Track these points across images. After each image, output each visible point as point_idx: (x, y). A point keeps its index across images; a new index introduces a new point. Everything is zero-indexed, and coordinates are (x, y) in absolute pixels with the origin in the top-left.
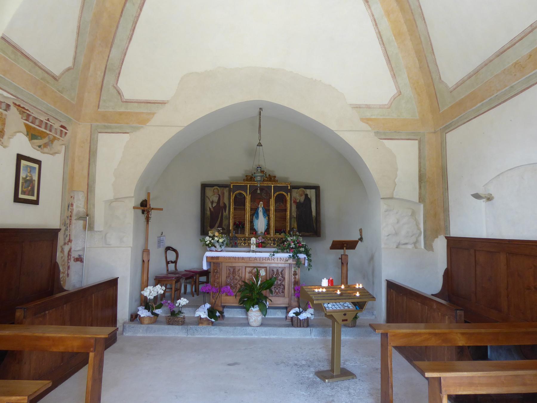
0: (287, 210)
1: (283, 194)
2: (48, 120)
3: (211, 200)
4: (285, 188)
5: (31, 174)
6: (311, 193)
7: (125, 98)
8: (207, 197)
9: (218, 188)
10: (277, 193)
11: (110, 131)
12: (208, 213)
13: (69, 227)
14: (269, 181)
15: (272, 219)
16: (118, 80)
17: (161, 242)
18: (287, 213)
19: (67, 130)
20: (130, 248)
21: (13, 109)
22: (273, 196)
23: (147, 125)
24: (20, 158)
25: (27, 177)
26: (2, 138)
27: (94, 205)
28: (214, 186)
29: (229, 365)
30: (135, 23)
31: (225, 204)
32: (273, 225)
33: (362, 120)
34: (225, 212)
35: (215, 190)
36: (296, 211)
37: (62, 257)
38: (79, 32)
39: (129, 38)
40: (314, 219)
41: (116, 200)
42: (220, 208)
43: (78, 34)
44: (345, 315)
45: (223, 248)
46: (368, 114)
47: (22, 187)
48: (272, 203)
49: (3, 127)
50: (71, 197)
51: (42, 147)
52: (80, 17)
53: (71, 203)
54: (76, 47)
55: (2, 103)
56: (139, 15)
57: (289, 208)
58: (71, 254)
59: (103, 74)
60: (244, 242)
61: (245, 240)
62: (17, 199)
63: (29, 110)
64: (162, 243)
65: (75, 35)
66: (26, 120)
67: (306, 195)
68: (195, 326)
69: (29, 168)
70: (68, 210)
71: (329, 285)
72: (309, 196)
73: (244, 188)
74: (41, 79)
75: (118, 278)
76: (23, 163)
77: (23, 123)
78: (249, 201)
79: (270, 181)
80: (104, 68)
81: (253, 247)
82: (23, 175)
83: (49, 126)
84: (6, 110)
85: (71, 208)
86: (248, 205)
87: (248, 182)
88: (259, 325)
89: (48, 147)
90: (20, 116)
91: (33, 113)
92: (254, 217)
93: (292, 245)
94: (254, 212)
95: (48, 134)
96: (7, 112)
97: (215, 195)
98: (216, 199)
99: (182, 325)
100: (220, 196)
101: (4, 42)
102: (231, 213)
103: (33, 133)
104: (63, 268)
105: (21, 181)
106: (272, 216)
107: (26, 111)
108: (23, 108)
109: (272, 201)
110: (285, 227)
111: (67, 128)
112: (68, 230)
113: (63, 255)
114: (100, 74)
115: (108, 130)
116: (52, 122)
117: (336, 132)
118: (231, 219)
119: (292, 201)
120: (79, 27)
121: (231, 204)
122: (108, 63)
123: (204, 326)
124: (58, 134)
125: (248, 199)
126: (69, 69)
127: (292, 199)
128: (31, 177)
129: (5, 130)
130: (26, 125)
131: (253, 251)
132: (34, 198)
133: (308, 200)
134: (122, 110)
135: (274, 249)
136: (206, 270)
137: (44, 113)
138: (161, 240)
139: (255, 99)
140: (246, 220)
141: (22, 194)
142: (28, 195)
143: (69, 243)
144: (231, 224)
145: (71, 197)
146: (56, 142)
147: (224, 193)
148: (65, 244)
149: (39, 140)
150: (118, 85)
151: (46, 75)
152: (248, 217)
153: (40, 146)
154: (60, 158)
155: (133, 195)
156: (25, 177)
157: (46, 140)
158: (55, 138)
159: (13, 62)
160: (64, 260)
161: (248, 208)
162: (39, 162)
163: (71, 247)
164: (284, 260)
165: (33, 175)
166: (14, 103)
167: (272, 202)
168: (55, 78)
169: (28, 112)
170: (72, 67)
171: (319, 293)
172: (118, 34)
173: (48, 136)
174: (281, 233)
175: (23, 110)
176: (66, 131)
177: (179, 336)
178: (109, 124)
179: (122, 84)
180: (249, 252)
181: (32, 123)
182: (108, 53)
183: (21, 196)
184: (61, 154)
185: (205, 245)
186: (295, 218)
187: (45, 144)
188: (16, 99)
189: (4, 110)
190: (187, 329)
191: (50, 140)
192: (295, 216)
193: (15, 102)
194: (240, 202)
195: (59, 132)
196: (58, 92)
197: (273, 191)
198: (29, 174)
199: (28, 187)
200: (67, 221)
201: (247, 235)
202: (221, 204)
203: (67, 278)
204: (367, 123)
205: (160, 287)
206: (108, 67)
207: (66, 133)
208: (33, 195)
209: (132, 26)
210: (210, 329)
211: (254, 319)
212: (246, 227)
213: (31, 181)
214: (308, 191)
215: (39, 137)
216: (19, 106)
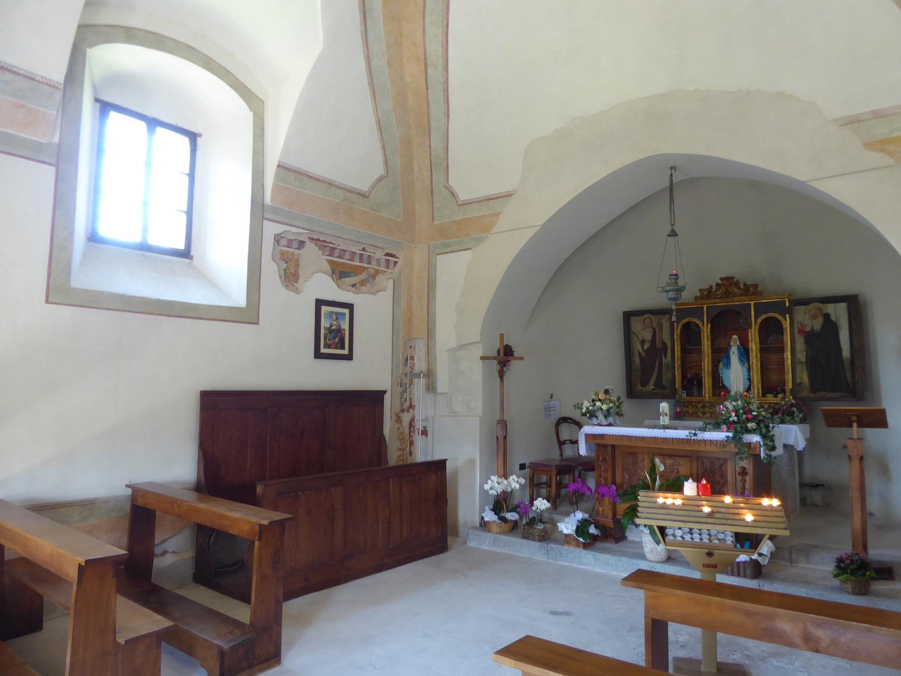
0: (785, 349)
1: (774, 318)
2: (364, 249)
3: (640, 337)
4: (779, 307)
5: (337, 322)
6: (839, 312)
7: (461, 200)
8: (634, 333)
9: (652, 317)
10: (764, 317)
11: (448, 250)
12: (637, 360)
13: (410, 387)
14: (745, 296)
15: (754, 367)
16: (448, 177)
17: (551, 409)
18: (785, 354)
19: (397, 258)
20: (478, 418)
21: (310, 246)
22: (753, 324)
23: (491, 232)
24: (320, 303)
25: (331, 326)
26: (296, 282)
27: (435, 357)
28: (812, 302)
29: (553, 613)
30: (446, 91)
31: (664, 343)
32: (757, 378)
33: (870, 145)
34: (666, 358)
35: (646, 321)
36: (805, 350)
37: (399, 429)
38: (380, 128)
39: (446, 115)
40: (847, 364)
41: (461, 347)
42: (655, 351)
43: (380, 130)
44: (710, 554)
45: (611, 419)
46: (882, 131)
47: (325, 338)
48: (753, 337)
49: (296, 269)
50: (411, 347)
51: (358, 285)
52: (376, 109)
53: (409, 355)
54: (384, 148)
55: (294, 242)
56: (447, 78)
57: (789, 344)
59: (429, 173)
60: (703, 410)
61: (704, 407)
62: (318, 355)
63: (333, 242)
64: (552, 410)
65: (376, 134)
66: (330, 255)
67: (827, 317)
68: (559, 546)
69: (334, 315)
70: (406, 365)
71: (698, 494)
72: (833, 318)
73: (697, 313)
74: (343, 200)
75: (447, 460)
76: (324, 309)
78: (707, 335)
79: (747, 295)
80: (429, 165)
82: (325, 323)
83: (365, 258)
84: (298, 249)
85: (411, 361)
86: (706, 342)
87: (704, 302)
88: (662, 560)
89: (368, 285)
90: (321, 252)
91: (338, 245)
92: (721, 365)
93: (734, 418)
94: (720, 355)
95: (365, 268)
97: (647, 329)
98: (648, 336)
99: (540, 541)
100: (655, 331)
101: (283, 170)
102: (676, 358)
103: (342, 270)
104: (401, 443)
105: (323, 332)
106: (754, 361)
107: (327, 244)
108: (324, 241)
109: (753, 336)
110: (783, 383)
112: (406, 392)
113: (399, 426)
114: (426, 173)
115: (448, 249)
116: (370, 251)
117: (811, 184)
118: (676, 369)
119: (796, 331)
120: (379, 121)
121: (676, 342)
122: (432, 157)
123: (572, 548)
124: (382, 265)
125: (706, 331)
126: (381, 179)
127: (795, 325)
128: (339, 325)
129: (299, 272)
130: (330, 262)
131: (665, 427)
132: (346, 352)
133: (830, 325)
134: (461, 217)
135: (700, 424)
136: (584, 456)
137: (355, 242)
138: (551, 406)
139: (647, 156)
140: (704, 370)
141: (325, 347)
142: (336, 349)
143: (410, 409)
144: (677, 379)
145: (411, 347)
146: (380, 277)
147: (662, 324)
148: (403, 411)
149: (352, 277)
150: (450, 183)
151: (349, 194)
152: (706, 365)
153: (353, 286)
154: (384, 299)
155: (478, 339)
156: (328, 326)
157: (363, 276)
158: (377, 272)
159: (300, 190)
160: (402, 433)
161: (706, 349)
162: (350, 307)
163: (414, 415)
164: (718, 446)
165: (341, 322)
166: (309, 238)
167: (753, 334)
168: (362, 195)
169: (331, 245)
170: (386, 175)
171: (664, 507)
172: (432, 114)
173: (366, 271)
174: (778, 393)
175: (324, 244)
176: (396, 260)
177: (536, 558)
178: (449, 240)
179: (453, 182)
180: (655, 427)
181: (339, 257)
182: (428, 144)
183: (323, 350)
184: (388, 290)
186: (802, 363)
187: (363, 281)
189: (296, 249)
190: (546, 549)
191: (370, 275)
192: (803, 360)
193: (312, 236)
194: (690, 335)
195: (383, 263)
196: (371, 211)
197: (753, 313)
198: (334, 323)
199: (335, 338)
200: (405, 381)
201: (707, 398)
202: (658, 344)
203: (408, 457)
204: (882, 151)
205: (516, 479)
206: (432, 162)
207: (396, 263)
208: (343, 348)
209: (444, 97)
210: (579, 555)
211: (649, 548)
212: (705, 382)
213: (339, 331)
214: (830, 308)
215: (353, 274)
216: (318, 240)
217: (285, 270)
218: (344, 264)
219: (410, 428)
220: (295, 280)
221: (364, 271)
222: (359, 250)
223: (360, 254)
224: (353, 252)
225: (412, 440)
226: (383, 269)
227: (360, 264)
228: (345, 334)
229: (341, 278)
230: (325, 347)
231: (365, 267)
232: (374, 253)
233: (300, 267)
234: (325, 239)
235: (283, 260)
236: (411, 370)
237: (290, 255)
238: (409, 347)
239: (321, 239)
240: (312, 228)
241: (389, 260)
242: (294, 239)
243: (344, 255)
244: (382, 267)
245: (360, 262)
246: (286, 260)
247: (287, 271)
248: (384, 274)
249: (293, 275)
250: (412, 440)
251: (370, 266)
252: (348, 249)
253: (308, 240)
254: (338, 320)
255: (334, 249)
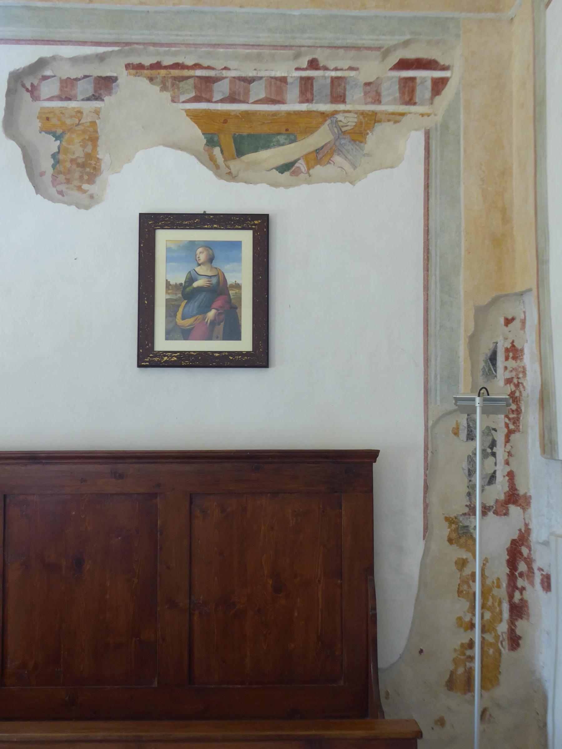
2: (313, 64)
19: (445, 68)
25: (191, 280)
49: (89, 149)
51: (301, 165)
58: (530, 554)
63: (205, 63)
66: (197, 99)
77: (184, 114)
81: (471, 665)
84: (96, 97)
85: (512, 363)
91: (226, 68)
95: (324, 116)
96: (103, 100)
107: (186, 73)
108: (176, 66)
111: (442, 62)
112: (494, 454)
129: (100, 156)
130: (195, 116)
141: (169, 336)
143: (513, 508)
153: (284, 168)
166: (128, 66)
169: (199, 73)
173: (329, 121)
181: (232, 99)
185: (486, 437)
187: (317, 151)
188: (119, 50)
191: (344, 133)
193: (136, 60)
203: (505, 651)
215: (282, 139)
216: (157, 66)
217: (54, 156)
218: (246, 116)
219: (512, 564)
220: (86, 177)
221: (322, 123)
222: (297, 69)
223: (302, 78)
224: (276, 78)
225: (522, 600)
226: (391, 108)
227: (304, 107)
228: (239, 299)
229: (240, 153)
230: (169, 336)
231: (322, 113)
232: (351, 69)
233: (100, 142)
234: (179, 60)
235: (48, 132)
236: (510, 388)
237: (71, 117)
238: (502, 321)
239: (166, 63)
240: (126, 37)
241: (413, 79)
242: (80, 76)
243: (247, 92)
244: (388, 103)
245: (302, 102)
246: (59, 131)
247: (61, 157)
248: (396, 122)
249: (78, 165)
250: (522, 600)
251: (341, 107)
252: (260, 74)
253: (125, 72)
254: (214, 264)
255: (209, 81)
